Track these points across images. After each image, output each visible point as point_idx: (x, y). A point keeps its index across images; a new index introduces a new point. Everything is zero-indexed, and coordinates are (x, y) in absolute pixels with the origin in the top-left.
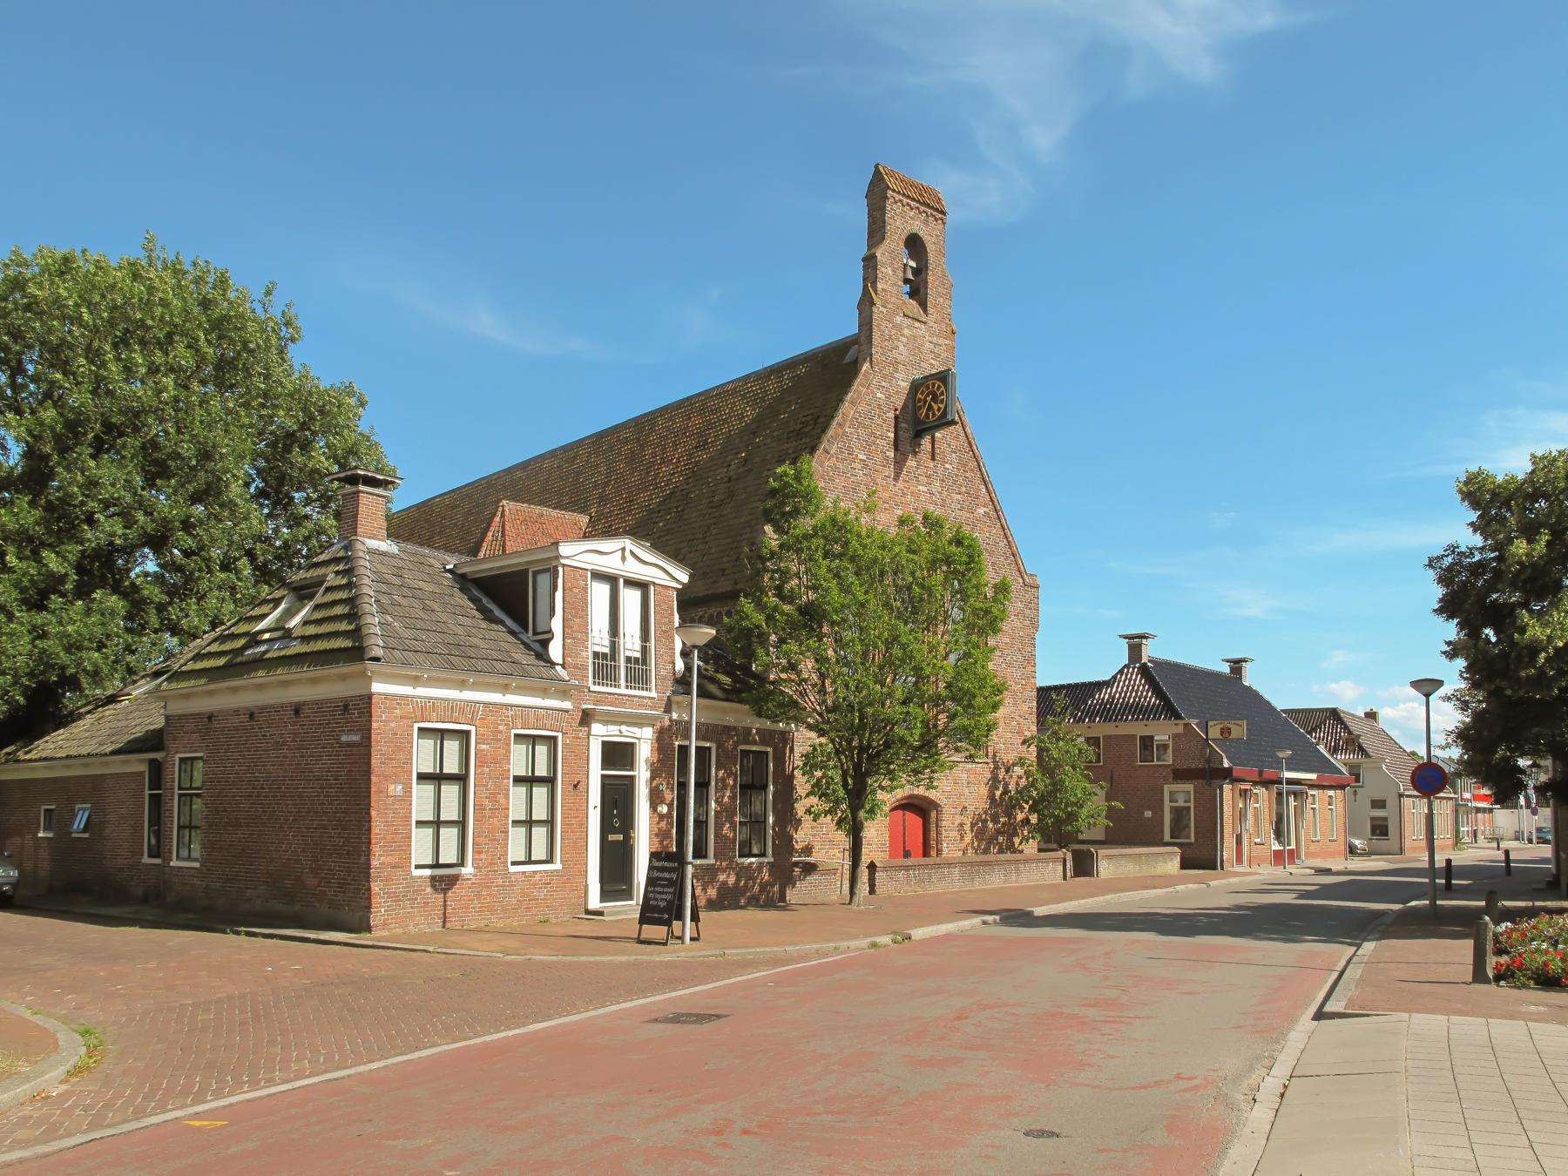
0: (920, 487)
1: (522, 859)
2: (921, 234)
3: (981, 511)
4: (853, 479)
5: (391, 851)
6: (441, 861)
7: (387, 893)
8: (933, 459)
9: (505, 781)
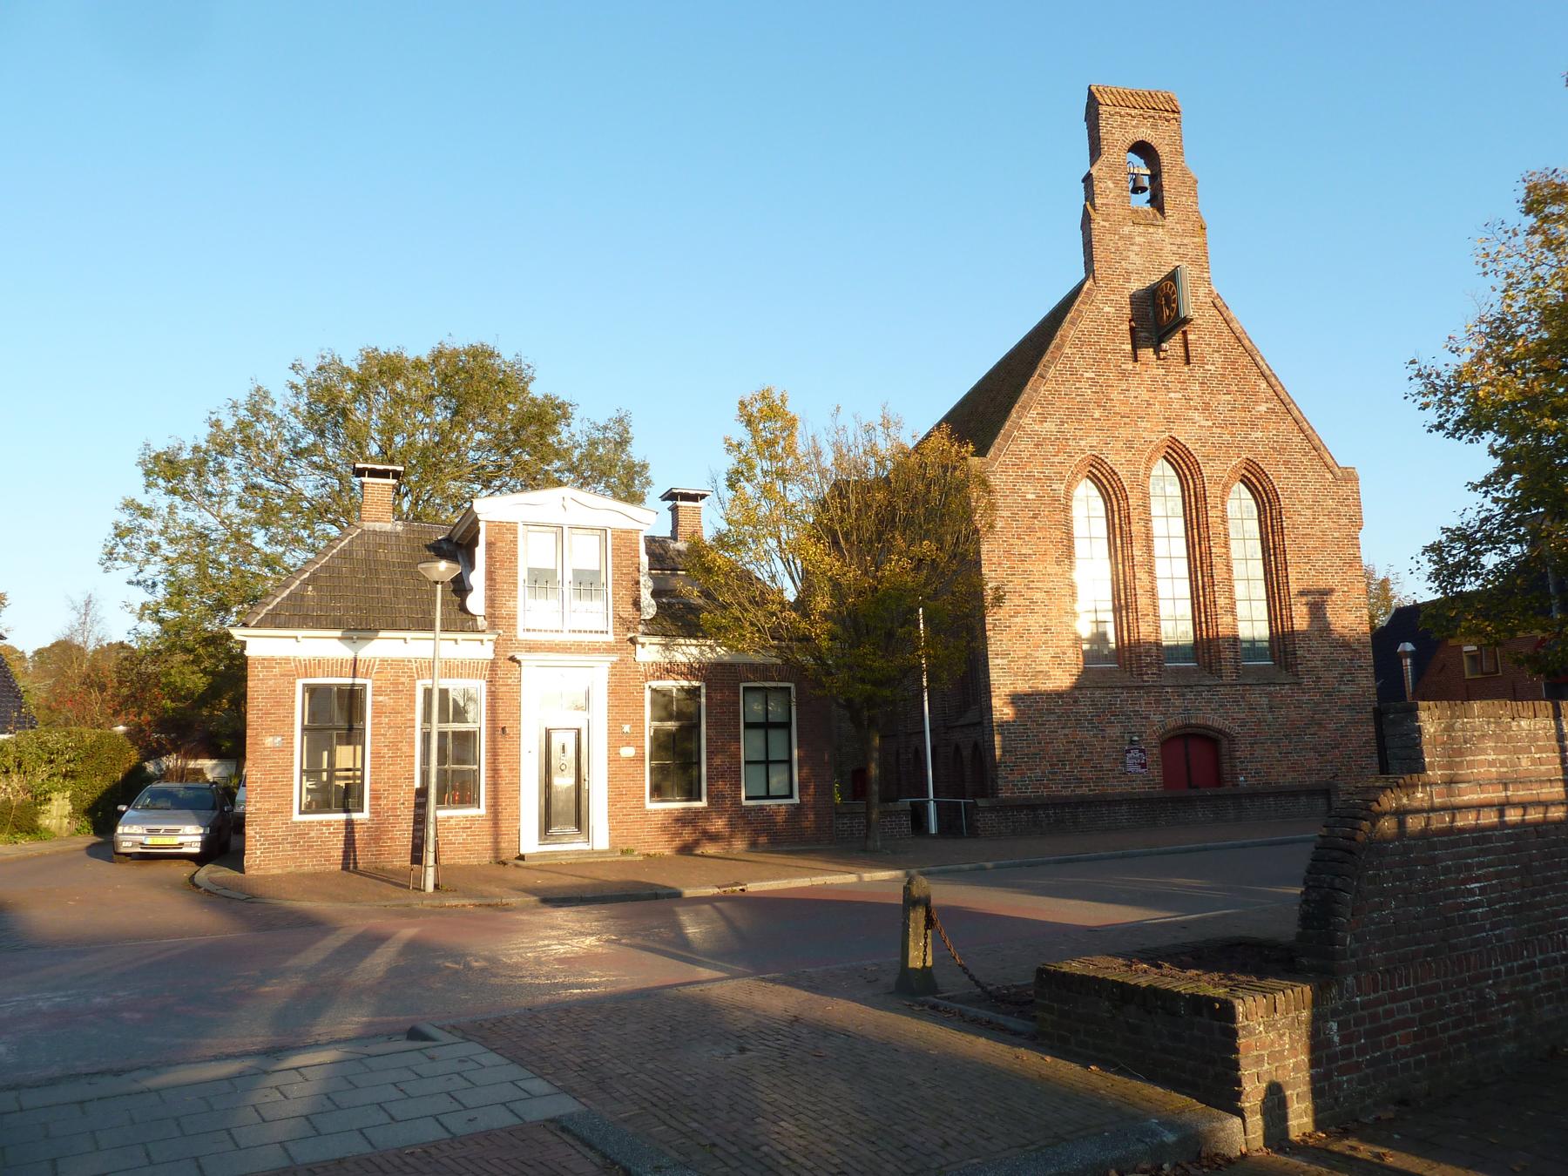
0: (1172, 395)
1: (763, 793)
2: (1148, 139)
3: (1263, 408)
4: (1078, 399)
5: (269, 797)
6: (771, 794)
7: (263, 836)
8: (1188, 362)
9: (408, 730)
